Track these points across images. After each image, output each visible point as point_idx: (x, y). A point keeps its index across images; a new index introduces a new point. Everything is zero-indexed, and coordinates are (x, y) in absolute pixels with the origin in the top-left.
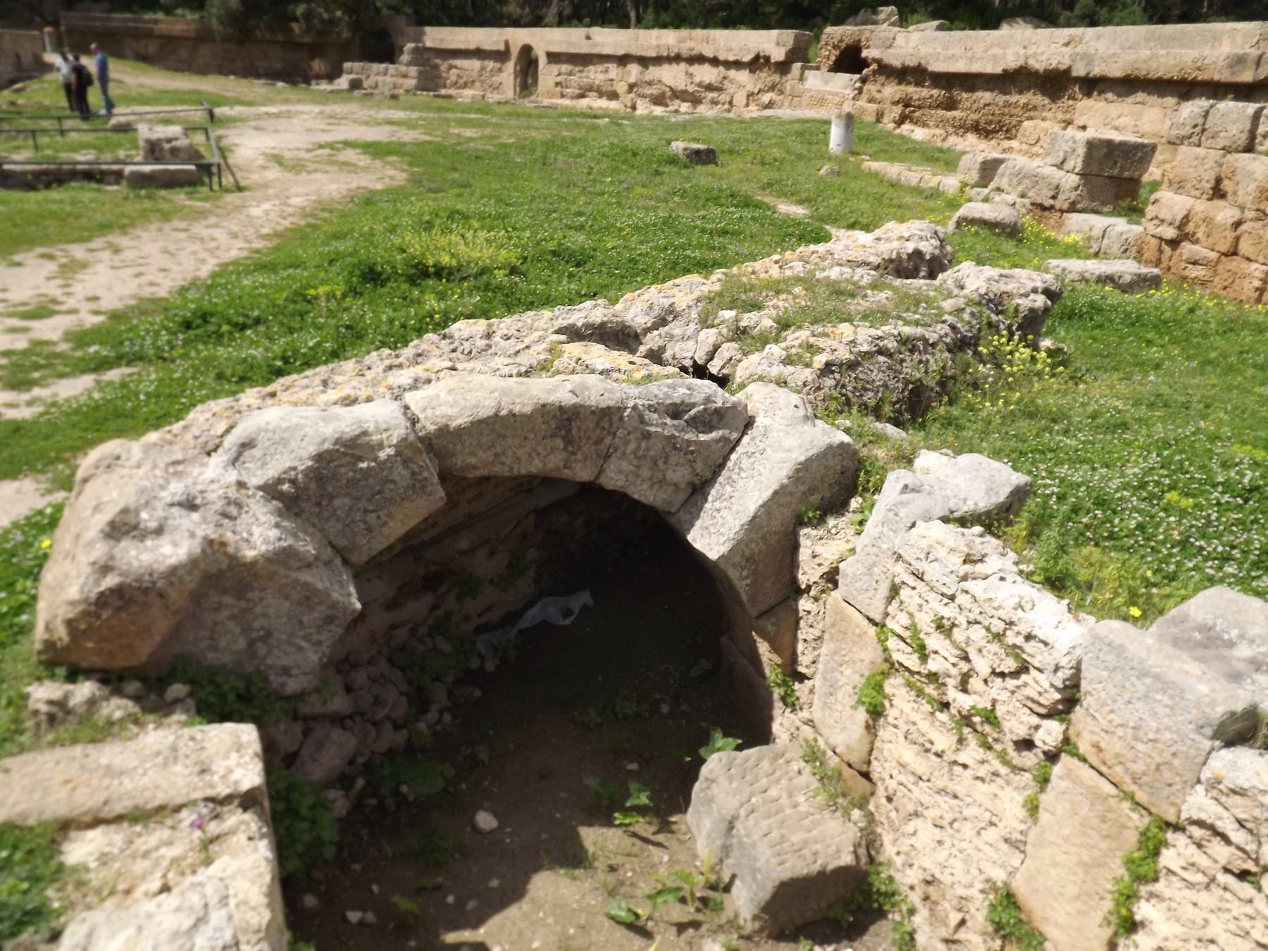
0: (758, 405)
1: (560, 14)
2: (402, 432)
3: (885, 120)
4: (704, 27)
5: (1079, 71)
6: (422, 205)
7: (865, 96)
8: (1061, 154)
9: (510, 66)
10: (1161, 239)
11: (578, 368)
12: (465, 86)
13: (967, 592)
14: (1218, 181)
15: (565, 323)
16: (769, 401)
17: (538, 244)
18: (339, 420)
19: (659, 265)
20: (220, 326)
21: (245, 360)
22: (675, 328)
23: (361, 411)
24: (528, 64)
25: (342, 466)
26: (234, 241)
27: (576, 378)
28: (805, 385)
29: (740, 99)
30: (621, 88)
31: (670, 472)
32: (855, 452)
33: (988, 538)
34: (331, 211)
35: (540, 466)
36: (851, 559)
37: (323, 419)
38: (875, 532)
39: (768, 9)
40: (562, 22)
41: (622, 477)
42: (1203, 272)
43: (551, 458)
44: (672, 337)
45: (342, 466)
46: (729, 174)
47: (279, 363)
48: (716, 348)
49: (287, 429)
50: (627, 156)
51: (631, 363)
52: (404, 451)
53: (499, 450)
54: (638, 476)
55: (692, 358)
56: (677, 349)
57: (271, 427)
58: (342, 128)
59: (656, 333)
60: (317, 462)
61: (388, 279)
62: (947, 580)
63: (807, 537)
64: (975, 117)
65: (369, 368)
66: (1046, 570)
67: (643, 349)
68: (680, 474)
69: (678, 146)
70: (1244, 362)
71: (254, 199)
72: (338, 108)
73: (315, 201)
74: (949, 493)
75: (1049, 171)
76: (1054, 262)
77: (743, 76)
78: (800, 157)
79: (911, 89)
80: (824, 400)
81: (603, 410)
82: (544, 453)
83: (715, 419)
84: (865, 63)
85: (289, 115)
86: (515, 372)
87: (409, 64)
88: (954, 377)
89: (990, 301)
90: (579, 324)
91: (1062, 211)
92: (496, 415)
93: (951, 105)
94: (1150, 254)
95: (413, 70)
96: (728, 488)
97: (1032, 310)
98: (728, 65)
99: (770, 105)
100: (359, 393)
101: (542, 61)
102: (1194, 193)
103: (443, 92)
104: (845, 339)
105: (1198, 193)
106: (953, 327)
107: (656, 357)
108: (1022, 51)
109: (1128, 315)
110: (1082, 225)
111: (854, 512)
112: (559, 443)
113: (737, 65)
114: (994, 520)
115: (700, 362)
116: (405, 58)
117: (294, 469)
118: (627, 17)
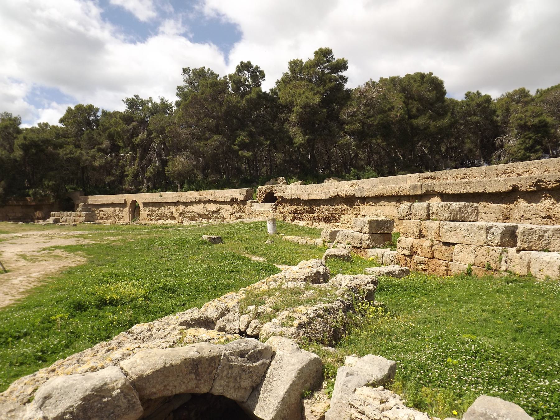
0: (276, 346)
1: (148, 187)
2: (123, 381)
3: (287, 219)
4: (209, 190)
5: (358, 195)
6: (97, 273)
7: (278, 211)
8: (360, 227)
9: (127, 209)
10: (404, 255)
11: (195, 340)
12: (107, 218)
13: (385, 417)
14: (420, 231)
15: (183, 320)
16: (280, 344)
17: (154, 285)
18: (92, 379)
19: (209, 288)
20: (7, 339)
21: (23, 354)
22: (229, 316)
23: (101, 374)
24: (135, 208)
25: (95, 402)
26: (6, 296)
27: (197, 344)
28: (292, 335)
29: (227, 216)
30: (176, 215)
31: (242, 382)
32: (321, 361)
33: (386, 391)
34: (52, 278)
35: (185, 388)
36: (329, 410)
37: (85, 380)
38: (339, 396)
39: (234, 181)
40: (149, 190)
41: (222, 388)
42: (424, 266)
43: (190, 384)
44: (228, 320)
45: (95, 402)
46: (229, 246)
47: (40, 354)
48: (249, 323)
49: (67, 387)
50: (184, 243)
51: (218, 335)
52: (124, 389)
53: (166, 383)
54: (228, 386)
55: (239, 328)
56: (231, 325)
57: (59, 387)
58: (52, 241)
59: (221, 319)
60: (83, 401)
61: (87, 308)
62: (375, 413)
63: (308, 405)
64: (322, 215)
65: (98, 352)
66: (413, 401)
67: (217, 327)
68: (246, 383)
69: (205, 237)
70: (451, 300)
71: (14, 276)
72: (50, 232)
73: (44, 274)
74: (365, 373)
75: (356, 233)
76: (368, 269)
77: (227, 207)
78: (256, 237)
79: (295, 207)
80: (301, 340)
81: (211, 357)
82: (186, 382)
83: (259, 355)
84: (276, 199)
85: (27, 236)
86: (168, 345)
87: (81, 211)
88: (347, 323)
89: (353, 289)
90: (189, 320)
91: (365, 248)
92: (164, 367)
93: (312, 212)
94: (402, 261)
95: (83, 214)
96: (269, 386)
97: (369, 290)
98: (221, 203)
99: (240, 217)
100: (97, 365)
101: (141, 206)
102: (413, 236)
103: (97, 221)
104: (304, 312)
105: (414, 237)
106: (342, 302)
107: (222, 329)
108: (336, 190)
109: (402, 287)
110: (374, 253)
111: (325, 388)
112: (193, 376)
113: (225, 203)
114: (386, 382)
115: (242, 330)
116: (80, 209)
117: (72, 406)
118: (177, 187)
